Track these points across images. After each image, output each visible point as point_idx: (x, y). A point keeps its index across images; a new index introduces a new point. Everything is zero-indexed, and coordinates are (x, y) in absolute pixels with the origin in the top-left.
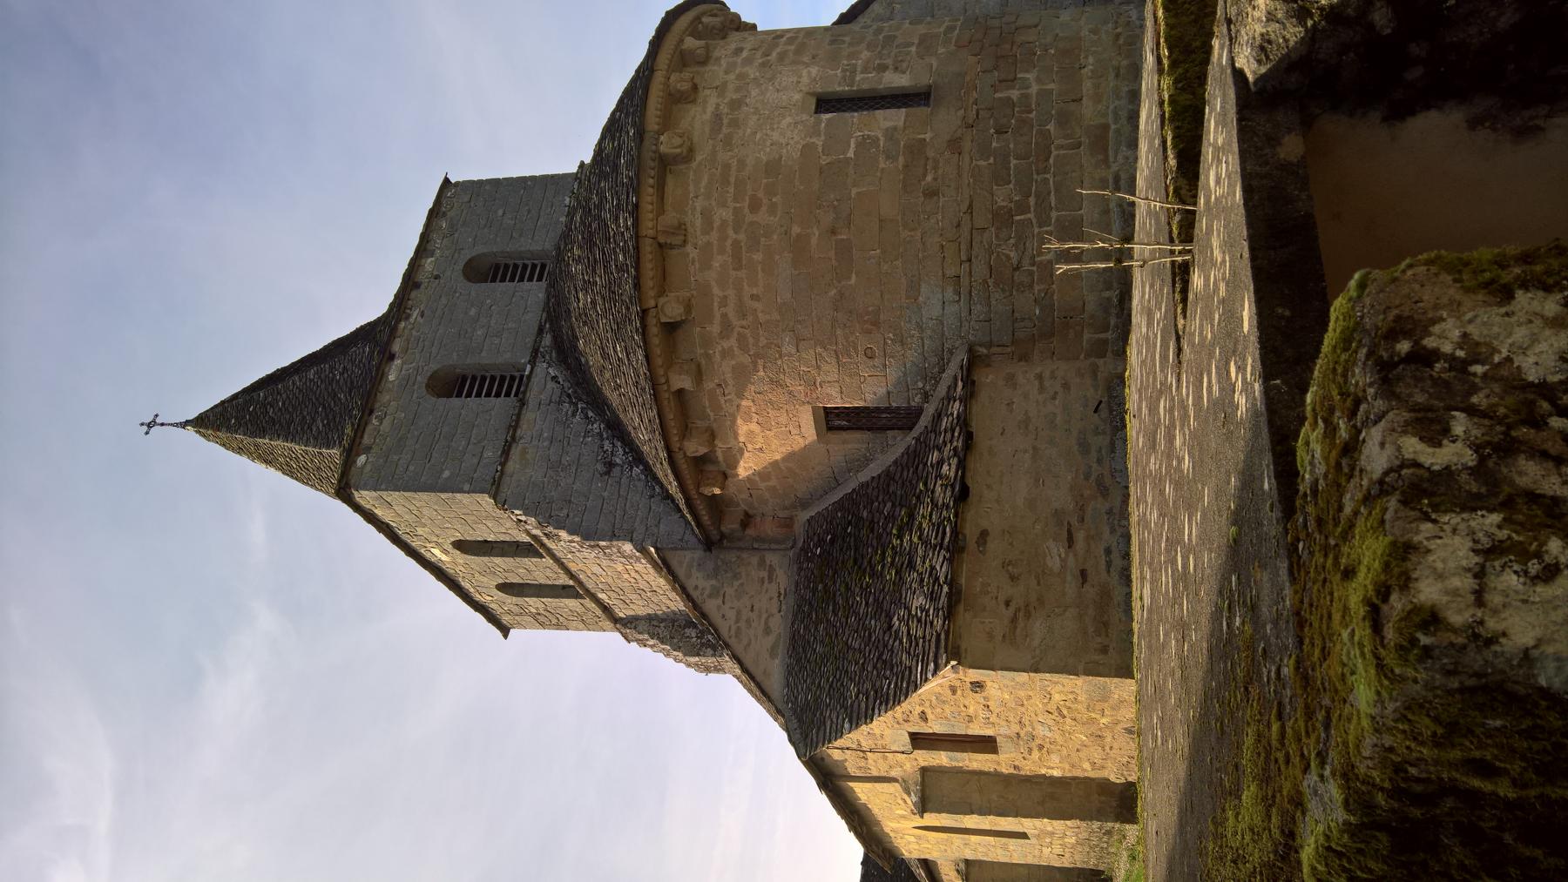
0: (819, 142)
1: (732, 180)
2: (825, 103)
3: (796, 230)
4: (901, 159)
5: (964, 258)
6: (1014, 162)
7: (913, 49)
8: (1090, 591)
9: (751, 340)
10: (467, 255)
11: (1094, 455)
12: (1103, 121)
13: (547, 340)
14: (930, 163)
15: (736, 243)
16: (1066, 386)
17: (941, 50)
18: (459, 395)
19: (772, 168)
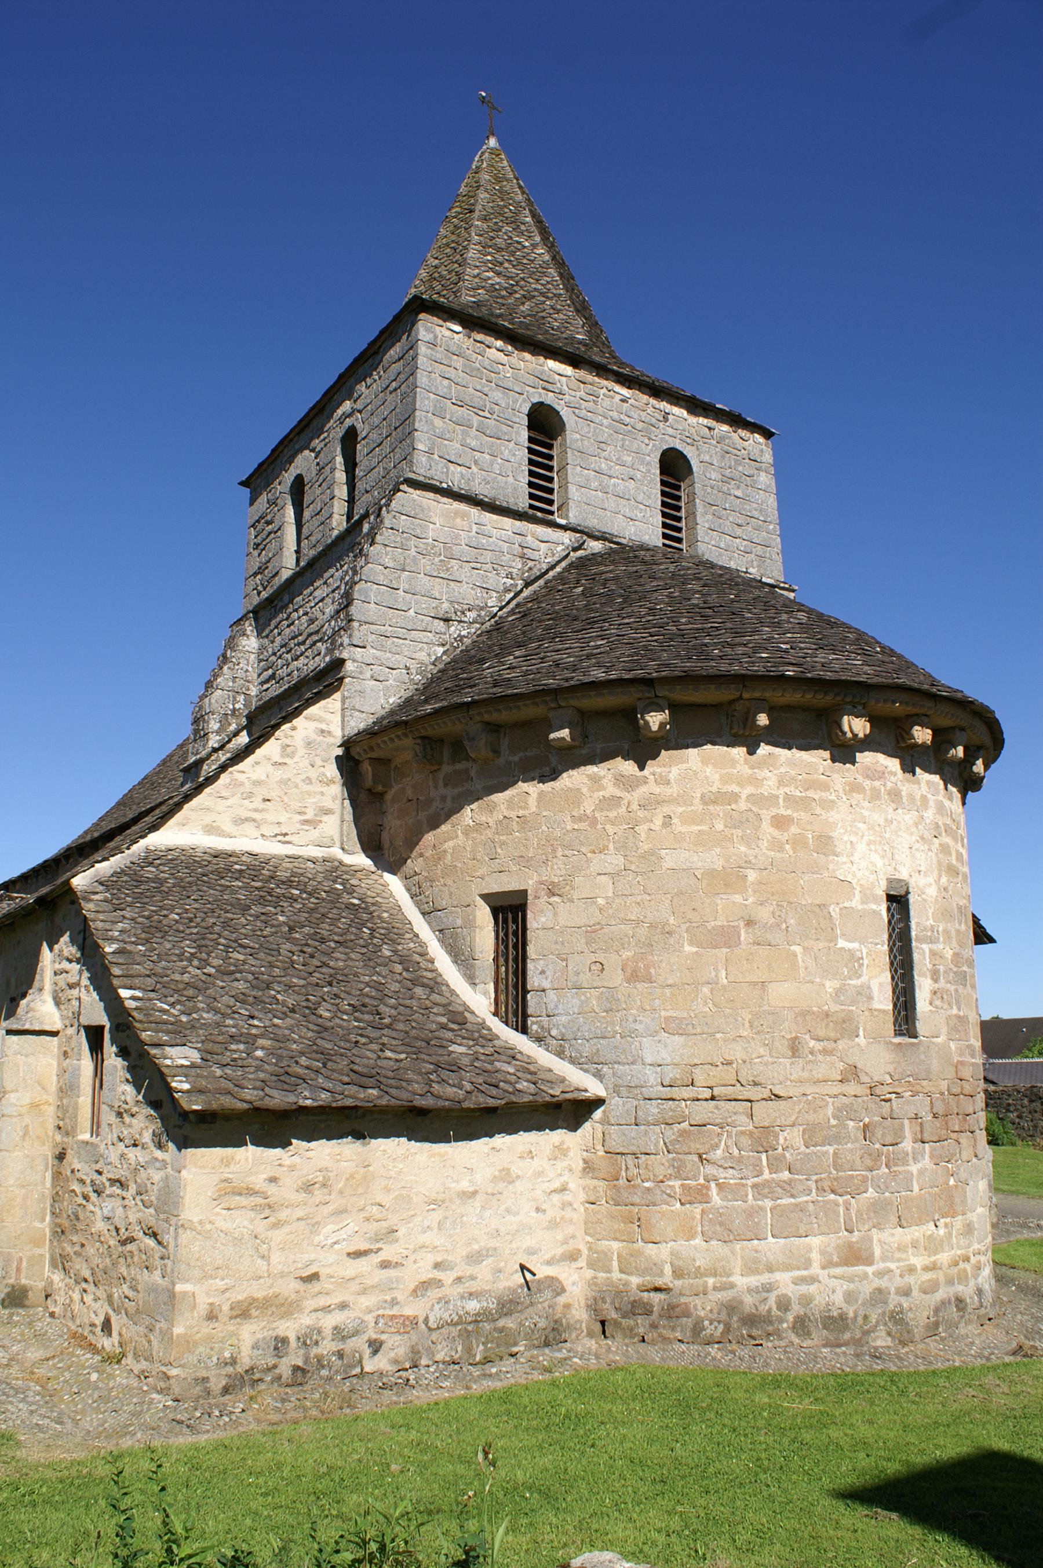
0: (855, 903)
1: (811, 794)
2: (898, 902)
3: (752, 876)
4: (834, 1008)
5: (717, 1091)
6: (831, 1150)
7: (955, 1011)
8: (289, 1287)
9: (612, 814)
10: (689, 452)
11: (470, 1271)
12: (877, 1252)
13: (595, 546)
14: (830, 1045)
15: (735, 797)
16: (553, 1225)
17: (953, 1045)
18: (531, 440)
19: (825, 844)
